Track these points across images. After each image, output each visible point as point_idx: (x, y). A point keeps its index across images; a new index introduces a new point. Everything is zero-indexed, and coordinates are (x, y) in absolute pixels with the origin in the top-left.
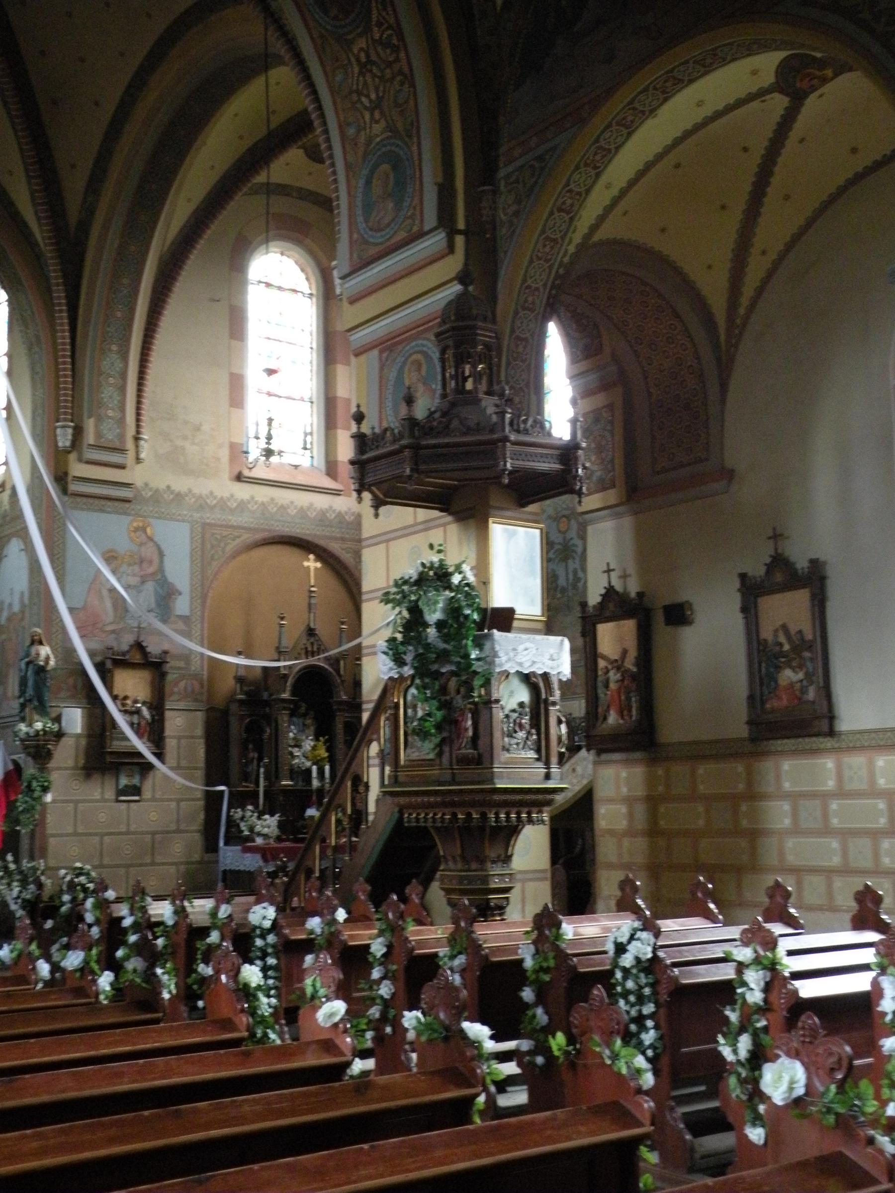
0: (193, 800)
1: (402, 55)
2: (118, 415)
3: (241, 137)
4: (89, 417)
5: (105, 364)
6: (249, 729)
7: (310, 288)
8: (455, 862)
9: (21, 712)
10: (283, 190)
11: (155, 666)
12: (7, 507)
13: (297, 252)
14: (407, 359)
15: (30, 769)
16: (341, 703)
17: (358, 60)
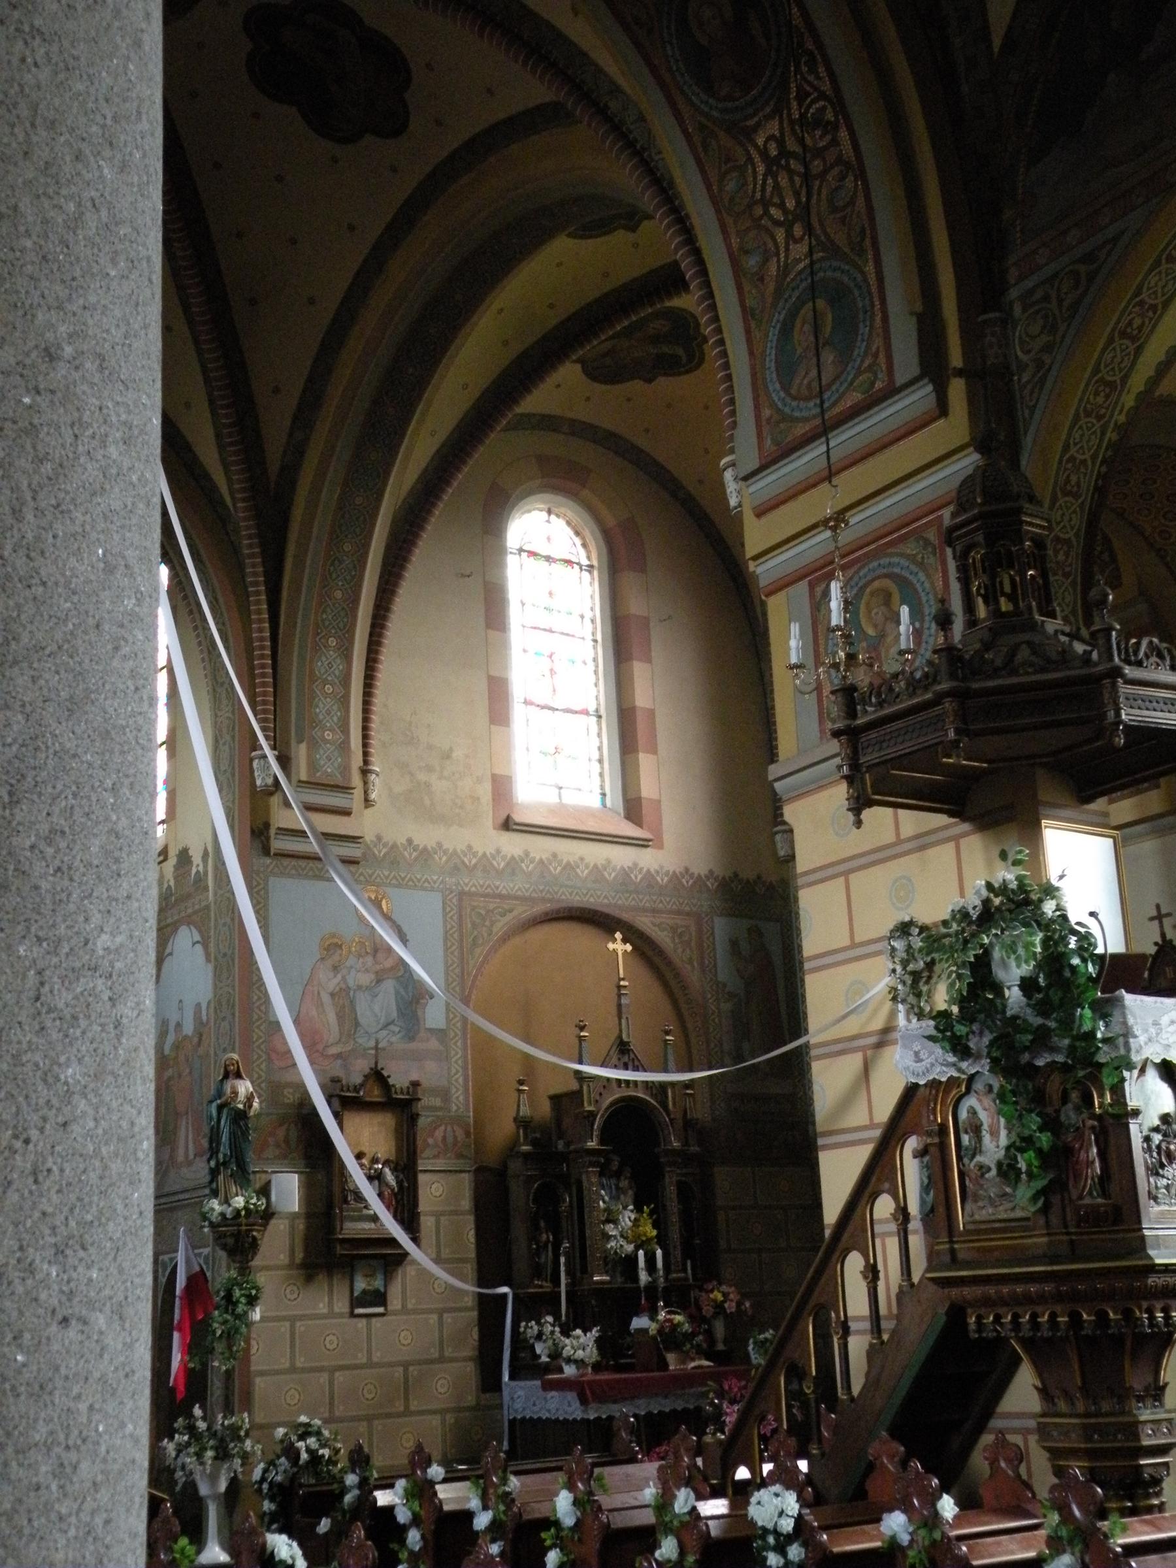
0: (460, 1310)
1: (843, 134)
2: (340, 737)
3: (506, 343)
4: (300, 741)
5: (320, 666)
7: (589, 558)
8: (1070, 1399)
9: (211, 1182)
10: (547, 423)
11: (401, 1107)
12: (172, 883)
13: (571, 509)
14: (862, 590)
15: (223, 1273)
16: (674, 1152)
17: (764, 153)
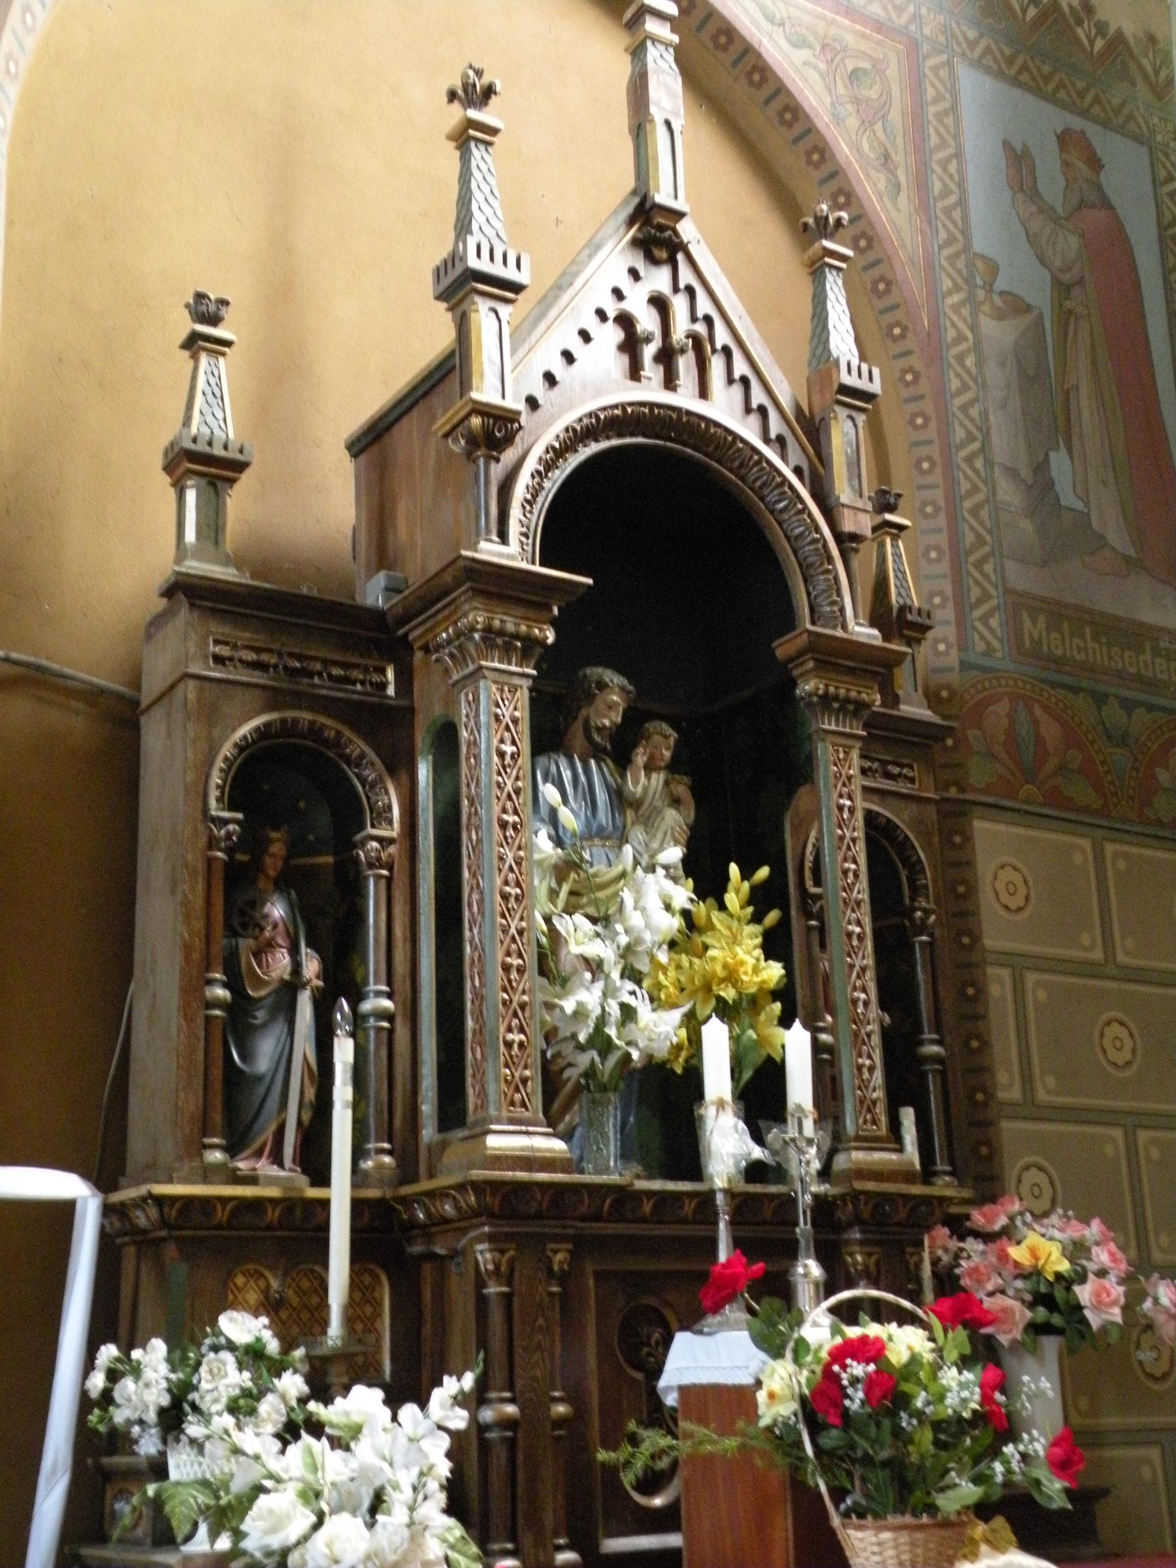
6: (261, 780)
